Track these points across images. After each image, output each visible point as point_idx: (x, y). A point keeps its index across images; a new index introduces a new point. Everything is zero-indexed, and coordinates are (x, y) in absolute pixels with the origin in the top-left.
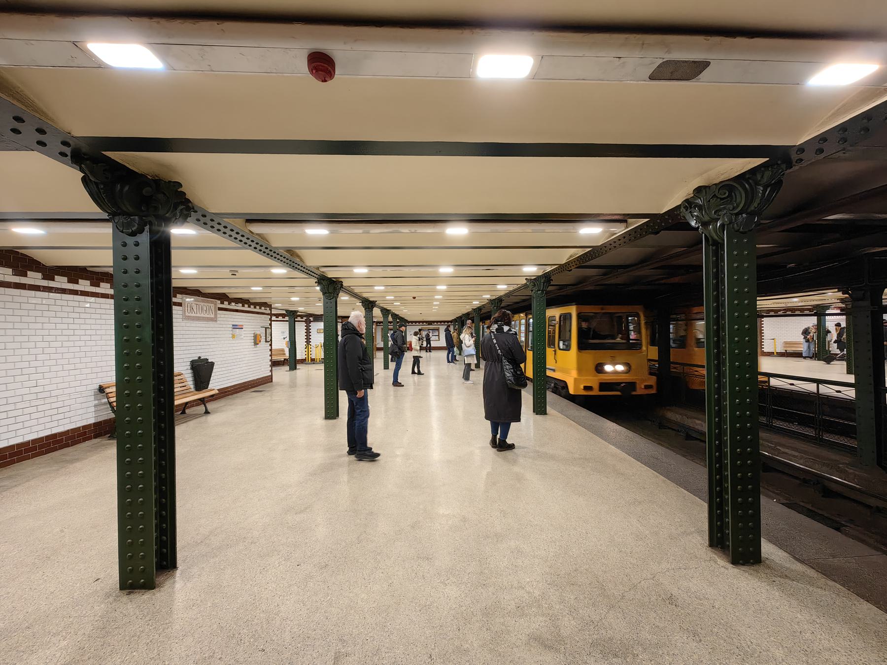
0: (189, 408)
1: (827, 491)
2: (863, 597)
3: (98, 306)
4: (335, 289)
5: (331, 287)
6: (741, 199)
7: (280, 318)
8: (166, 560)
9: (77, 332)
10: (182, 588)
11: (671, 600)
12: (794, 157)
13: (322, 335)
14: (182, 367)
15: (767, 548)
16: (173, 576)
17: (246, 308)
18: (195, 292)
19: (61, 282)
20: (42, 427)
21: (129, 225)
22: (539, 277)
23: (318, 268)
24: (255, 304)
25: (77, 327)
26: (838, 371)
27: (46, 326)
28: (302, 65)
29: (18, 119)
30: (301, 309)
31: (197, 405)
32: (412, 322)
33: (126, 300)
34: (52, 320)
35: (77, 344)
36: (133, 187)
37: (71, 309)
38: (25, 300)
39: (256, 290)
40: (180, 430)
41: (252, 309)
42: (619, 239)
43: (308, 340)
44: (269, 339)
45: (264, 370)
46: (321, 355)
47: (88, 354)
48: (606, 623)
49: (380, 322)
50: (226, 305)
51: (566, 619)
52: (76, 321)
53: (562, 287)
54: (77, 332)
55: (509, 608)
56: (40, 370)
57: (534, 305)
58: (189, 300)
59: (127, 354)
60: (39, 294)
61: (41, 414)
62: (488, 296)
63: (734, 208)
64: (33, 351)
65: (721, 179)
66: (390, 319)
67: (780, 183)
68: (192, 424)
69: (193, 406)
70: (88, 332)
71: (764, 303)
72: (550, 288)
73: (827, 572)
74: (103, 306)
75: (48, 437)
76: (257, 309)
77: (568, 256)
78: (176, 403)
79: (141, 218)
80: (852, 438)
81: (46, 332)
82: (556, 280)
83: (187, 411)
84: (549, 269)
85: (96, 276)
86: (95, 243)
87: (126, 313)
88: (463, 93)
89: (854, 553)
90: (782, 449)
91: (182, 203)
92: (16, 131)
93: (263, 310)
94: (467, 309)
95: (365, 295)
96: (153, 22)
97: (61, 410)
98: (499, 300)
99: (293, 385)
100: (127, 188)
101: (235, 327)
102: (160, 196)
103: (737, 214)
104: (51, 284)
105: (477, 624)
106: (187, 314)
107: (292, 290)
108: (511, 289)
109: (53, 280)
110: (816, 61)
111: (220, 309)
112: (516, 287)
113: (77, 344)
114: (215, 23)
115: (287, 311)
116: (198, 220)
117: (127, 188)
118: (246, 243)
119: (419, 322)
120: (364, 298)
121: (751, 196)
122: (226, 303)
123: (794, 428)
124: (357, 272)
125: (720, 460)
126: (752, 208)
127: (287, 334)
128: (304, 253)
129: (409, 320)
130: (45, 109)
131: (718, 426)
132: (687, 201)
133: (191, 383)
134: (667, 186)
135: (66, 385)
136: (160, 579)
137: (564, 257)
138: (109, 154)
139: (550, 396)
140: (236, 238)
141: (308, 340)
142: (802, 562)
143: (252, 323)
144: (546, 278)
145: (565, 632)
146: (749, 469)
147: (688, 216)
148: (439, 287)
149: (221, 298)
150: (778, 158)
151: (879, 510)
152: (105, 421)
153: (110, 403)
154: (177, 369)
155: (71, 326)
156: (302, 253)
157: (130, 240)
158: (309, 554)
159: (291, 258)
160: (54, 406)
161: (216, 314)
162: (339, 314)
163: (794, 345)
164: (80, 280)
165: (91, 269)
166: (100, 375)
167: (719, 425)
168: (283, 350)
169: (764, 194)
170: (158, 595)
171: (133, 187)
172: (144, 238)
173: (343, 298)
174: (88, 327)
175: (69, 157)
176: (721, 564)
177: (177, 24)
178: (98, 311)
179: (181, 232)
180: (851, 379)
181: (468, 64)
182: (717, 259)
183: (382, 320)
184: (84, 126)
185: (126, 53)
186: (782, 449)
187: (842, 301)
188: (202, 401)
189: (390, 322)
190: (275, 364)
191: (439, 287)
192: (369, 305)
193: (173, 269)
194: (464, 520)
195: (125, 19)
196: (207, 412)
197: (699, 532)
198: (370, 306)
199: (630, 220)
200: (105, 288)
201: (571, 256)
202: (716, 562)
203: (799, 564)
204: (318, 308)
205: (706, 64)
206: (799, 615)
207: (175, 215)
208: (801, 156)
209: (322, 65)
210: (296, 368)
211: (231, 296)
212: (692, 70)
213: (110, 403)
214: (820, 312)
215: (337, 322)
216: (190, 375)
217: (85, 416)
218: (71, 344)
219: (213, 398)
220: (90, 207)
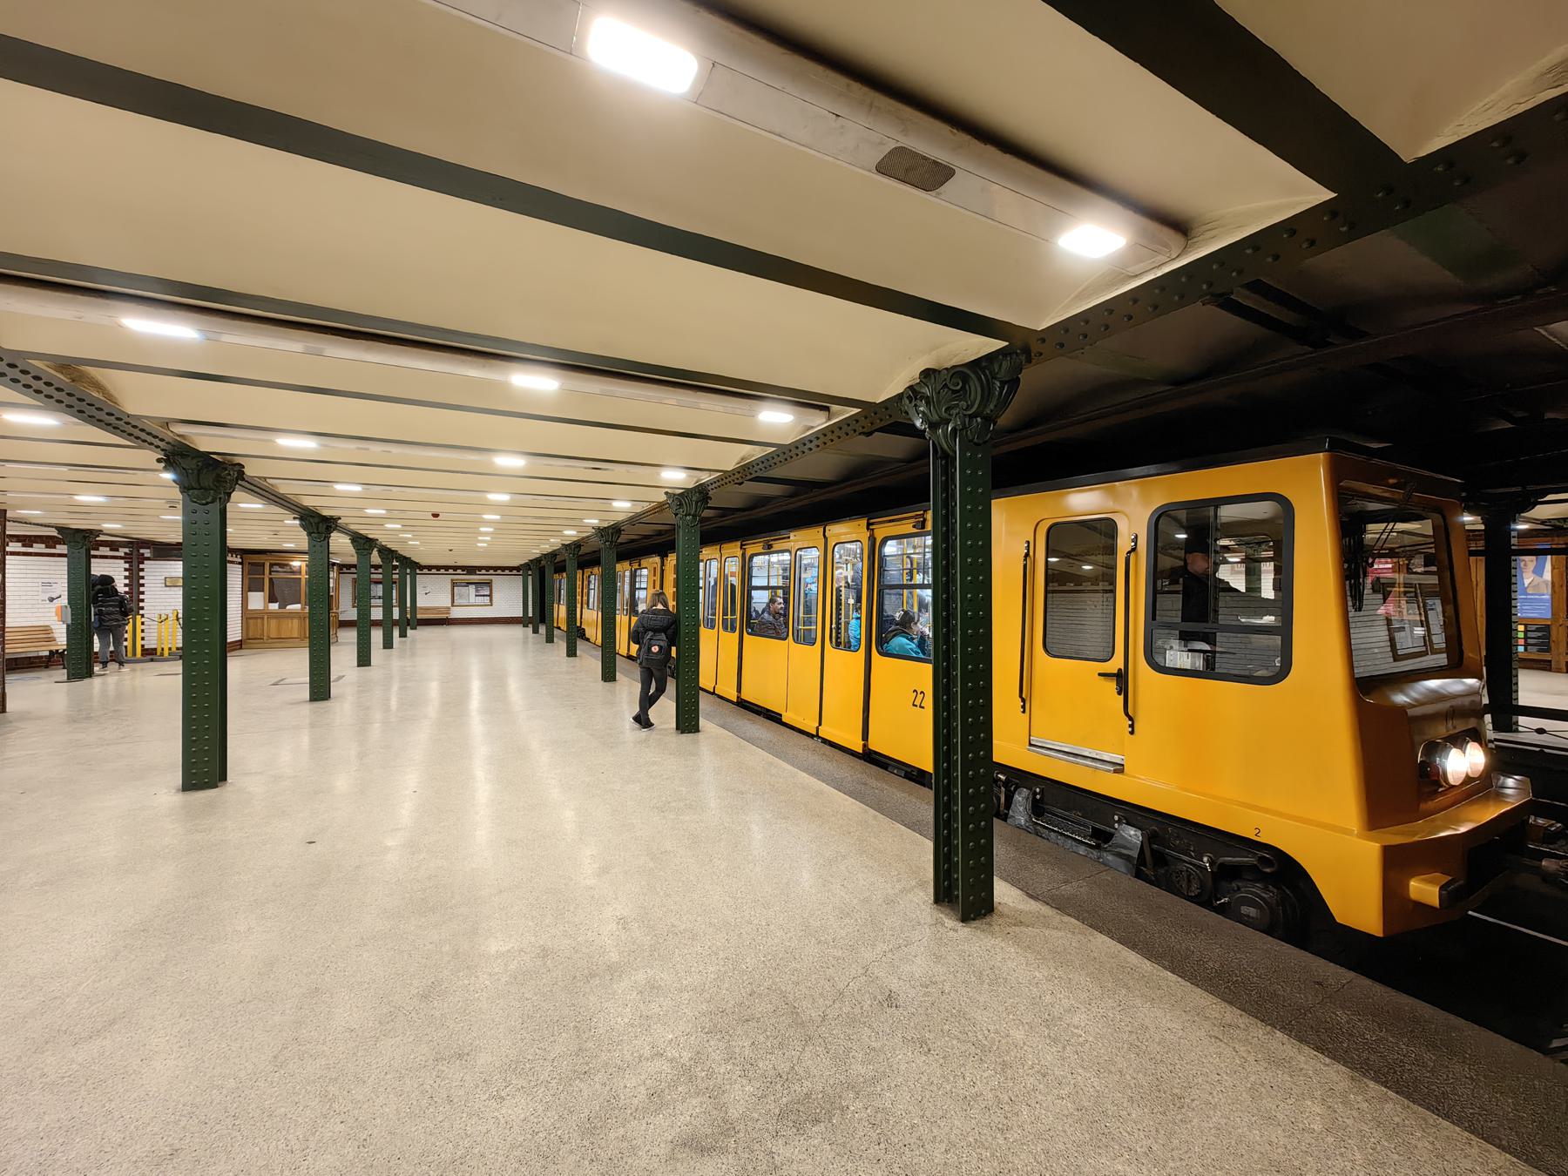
4: (219, 480)
5: (208, 478)
6: (975, 387)
12: (1036, 347)
13: (180, 592)
15: (1004, 892)
23: (166, 423)
32: (430, 568)
42: (817, 436)
46: (174, 637)
48: (801, 1071)
49: (349, 566)
51: (737, 1086)
53: (725, 512)
55: (635, 1101)
57: (681, 539)
62: (595, 522)
63: (968, 408)
65: (953, 363)
66: (375, 558)
72: (707, 513)
77: (738, 459)
84: (705, 478)
94: (551, 544)
95: (308, 502)
98: (616, 529)
103: (972, 417)
105: (572, 1158)
108: (639, 510)
112: (646, 506)
115: (60, 529)
119: (447, 568)
120: (306, 509)
129: (423, 562)
132: (911, 387)
137: (730, 458)
145: (734, 1113)
147: (912, 412)
150: (1021, 347)
159: (72, 388)
168: (47, 630)
173: (243, 505)
183: (354, 560)
189: (376, 567)
192: (319, 525)
194: (545, 953)
198: (322, 527)
199: (834, 408)
204: (168, 523)
210: (90, 674)
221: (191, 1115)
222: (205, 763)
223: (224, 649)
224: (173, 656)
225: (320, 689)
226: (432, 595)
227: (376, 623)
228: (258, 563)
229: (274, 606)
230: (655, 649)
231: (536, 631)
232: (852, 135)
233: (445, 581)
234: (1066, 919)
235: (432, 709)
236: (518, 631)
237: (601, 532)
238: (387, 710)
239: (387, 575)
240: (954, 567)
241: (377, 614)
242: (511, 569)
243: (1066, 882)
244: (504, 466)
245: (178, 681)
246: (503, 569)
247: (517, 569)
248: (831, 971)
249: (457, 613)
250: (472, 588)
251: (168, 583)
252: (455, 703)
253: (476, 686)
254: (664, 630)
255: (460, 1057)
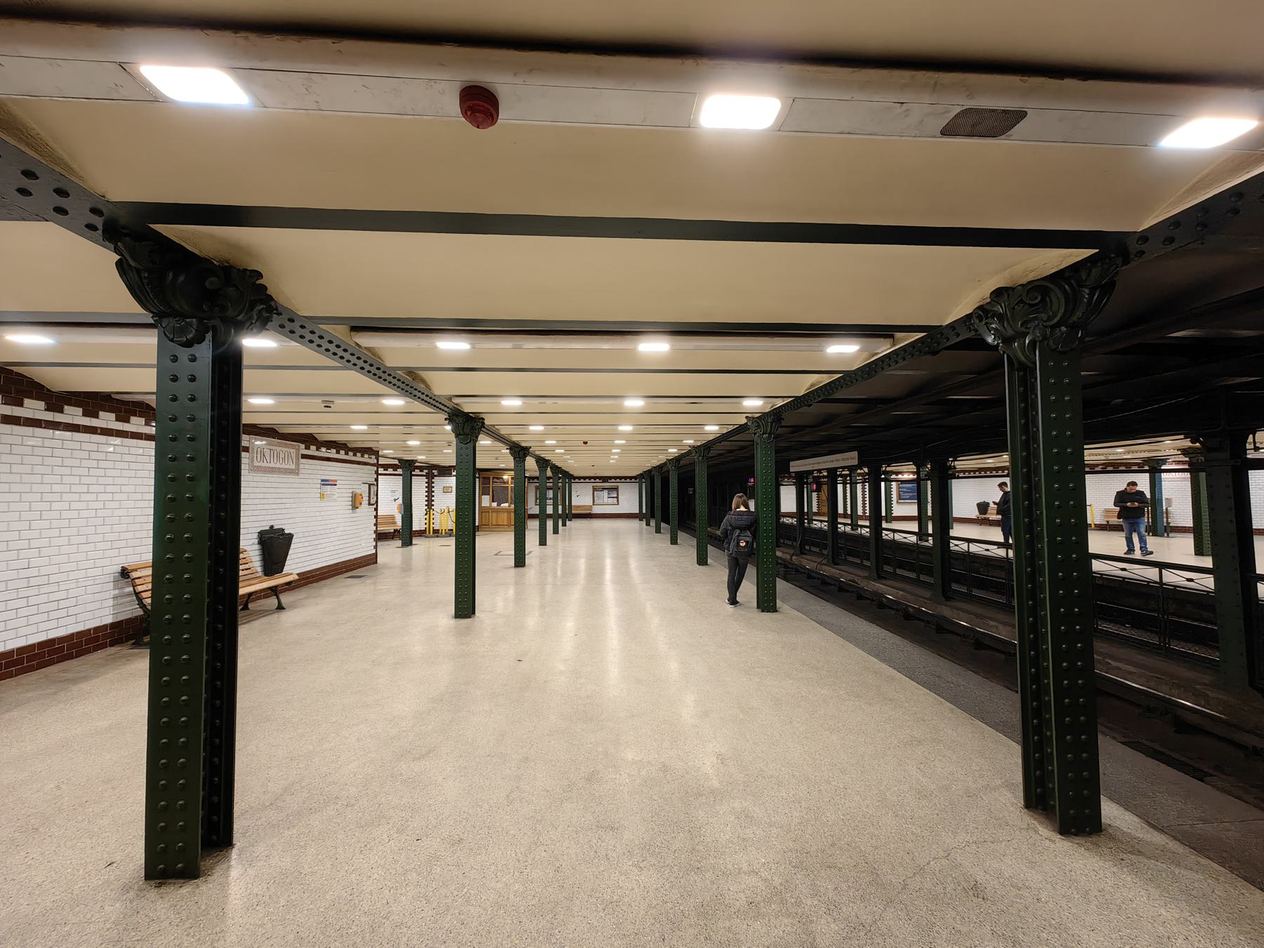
0: (253, 601)
1: (1183, 724)
2: (1253, 883)
3: (126, 450)
4: (473, 428)
5: (468, 426)
6: (1058, 304)
7: (390, 471)
8: (218, 835)
9: (92, 489)
10: (238, 878)
11: (976, 890)
12: (1134, 247)
14: (249, 544)
15: (1110, 811)
16: (228, 858)
17: (342, 455)
18: (268, 432)
19: (73, 415)
20: (33, 629)
21: (182, 331)
22: (764, 414)
23: (450, 398)
24: (356, 451)
25: (93, 480)
26: (997, 535)
27: (47, 479)
28: (452, 105)
29: (29, 174)
30: (421, 458)
31: (266, 597)
32: (580, 478)
33: (174, 440)
34: (57, 470)
35: (92, 505)
36: (191, 277)
37: (85, 455)
38: (18, 440)
39: (358, 430)
40: (246, 633)
41: (350, 457)
43: (430, 504)
44: (373, 501)
45: (365, 547)
46: (449, 523)
47: (108, 521)
48: (883, 927)
50: (313, 451)
51: (823, 921)
52: (93, 472)
53: (796, 429)
54: (92, 489)
56: (34, 544)
58: (259, 443)
59: (171, 520)
60: (39, 431)
61: (34, 610)
62: (691, 442)
63: (1050, 319)
64: (25, 516)
66: (549, 473)
67: (1112, 284)
68: (257, 624)
69: (260, 598)
70: (109, 489)
71: (1093, 454)
72: (780, 430)
73: (1201, 845)
74: (133, 451)
75: (41, 645)
76: (358, 458)
77: (808, 385)
78: (242, 591)
79: (200, 321)
80: (1211, 647)
81: (47, 488)
82: (790, 419)
83: (250, 606)
84: (780, 403)
85: (124, 407)
86: (132, 359)
87: (173, 460)
88: (680, 149)
89: (1229, 816)
90: (1113, 663)
91: (262, 301)
92: (23, 192)
93: (366, 458)
95: (515, 438)
96: (240, 38)
97: (63, 604)
98: (708, 446)
99: (407, 568)
100: (182, 278)
101: (325, 483)
102: (231, 290)
103: (1053, 327)
104: (58, 417)
105: (691, 931)
106: (256, 464)
107: (408, 430)
109: (62, 412)
110: (1169, 117)
111: (304, 456)
112: (731, 428)
113: (92, 505)
114: (329, 41)
115: (400, 460)
116: (282, 326)
117: (182, 278)
118: (348, 361)
119: (590, 478)
121: (1072, 301)
122: (313, 448)
123: (1126, 631)
124: (507, 404)
125: (1037, 678)
126: (1075, 318)
127: (399, 494)
128: (430, 377)
129: (576, 474)
130: (67, 159)
131: (1030, 631)
132: (980, 308)
133: (259, 564)
134: (951, 287)
135: (73, 566)
136: (209, 862)
137: (802, 385)
138: (159, 228)
139: (781, 585)
140: (335, 354)
141: (430, 504)
142: (1161, 830)
143: (350, 478)
144: (777, 414)
146: (1083, 694)
147: (982, 329)
148: (621, 428)
149: (309, 442)
150: (1111, 249)
151: (1256, 752)
152: (129, 621)
153: (137, 594)
154: (244, 543)
155: (84, 480)
156: (426, 375)
157: (183, 354)
158: (434, 822)
159: (409, 382)
160: (53, 597)
161: (298, 464)
162: (479, 465)
163: (1146, 514)
164: (101, 413)
165: (118, 397)
166: (123, 551)
167: (1034, 628)
168: (393, 517)
169: (1090, 299)
170: (204, 888)
171: (191, 277)
172: (205, 352)
173: (484, 442)
174: (110, 481)
175: (100, 232)
176: (1043, 836)
177: (273, 42)
178: (126, 458)
179: (255, 343)
180: (1208, 562)
181: (688, 108)
182: (1026, 390)
183: (537, 474)
184: (125, 185)
185: (195, 83)
186: (1113, 663)
187: (1185, 452)
188: (274, 591)
189: (549, 478)
190: (381, 537)
191: (621, 428)
192: (520, 452)
193: (244, 398)
194: (665, 769)
195: (198, 32)
196: (280, 607)
197: (1009, 786)
199: (898, 335)
200: (136, 424)
201: (812, 385)
202: (1036, 832)
203: (1156, 833)
204: (448, 456)
205: (1020, 115)
206: (1163, 911)
207: (251, 318)
208: (1143, 247)
209: (480, 104)
210: (411, 544)
211: (321, 438)
212: (1000, 123)
213: (137, 594)
214: (1154, 468)
215: (474, 478)
216: (257, 553)
217: (98, 614)
218: (84, 505)
219: (290, 586)
220: (129, 306)
221: (467, 819)
222: (465, 606)
223: (475, 529)
224: (449, 534)
225: (520, 561)
226: (581, 497)
227: (550, 516)
228: (489, 476)
229: (495, 504)
230: (743, 544)
231: (648, 524)
232: (926, 106)
233: (589, 487)
234: (1205, 861)
235: (582, 575)
236: (635, 524)
237: (695, 448)
238: (555, 576)
239: (555, 484)
240: (1037, 473)
241: (550, 510)
242: (631, 478)
243: (1205, 821)
244: (632, 406)
245: (1192, 541)
246: (626, 478)
247: (635, 478)
248: (910, 845)
249: (596, 510)
250: (606, 492)
251: (446, 490)
252: (595, 574)
253: (608, 563)
254: (747, 528)
255: (612, 829)
